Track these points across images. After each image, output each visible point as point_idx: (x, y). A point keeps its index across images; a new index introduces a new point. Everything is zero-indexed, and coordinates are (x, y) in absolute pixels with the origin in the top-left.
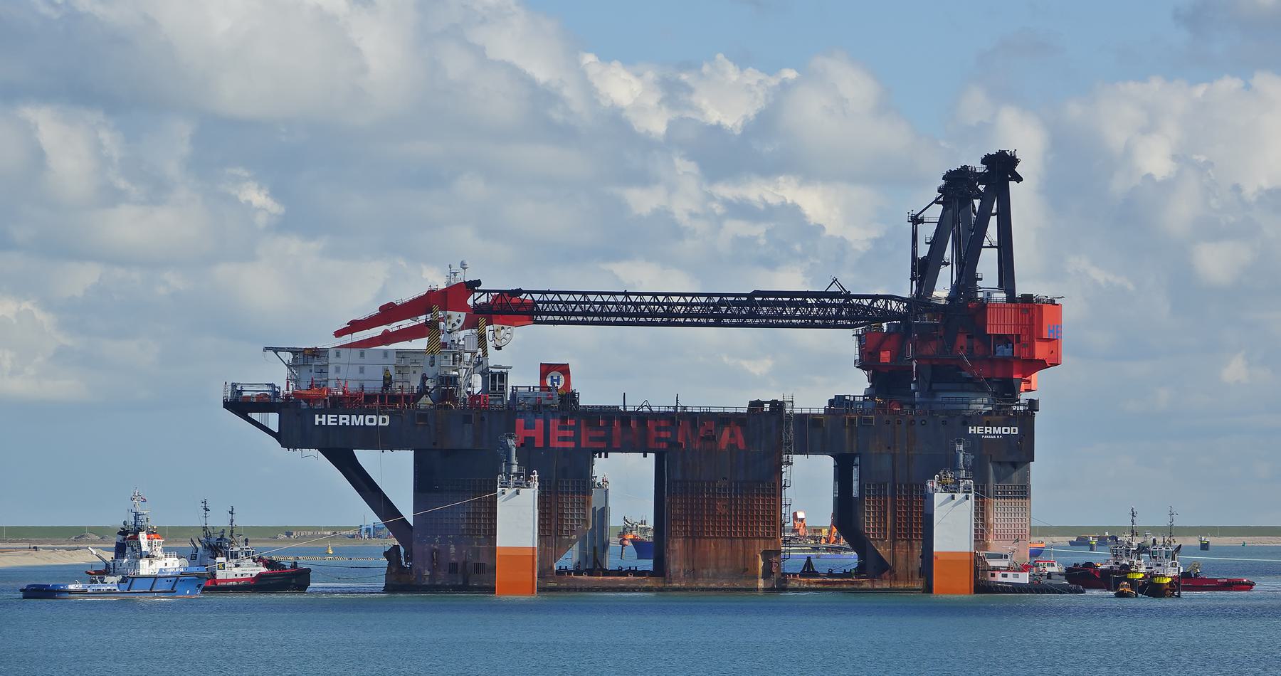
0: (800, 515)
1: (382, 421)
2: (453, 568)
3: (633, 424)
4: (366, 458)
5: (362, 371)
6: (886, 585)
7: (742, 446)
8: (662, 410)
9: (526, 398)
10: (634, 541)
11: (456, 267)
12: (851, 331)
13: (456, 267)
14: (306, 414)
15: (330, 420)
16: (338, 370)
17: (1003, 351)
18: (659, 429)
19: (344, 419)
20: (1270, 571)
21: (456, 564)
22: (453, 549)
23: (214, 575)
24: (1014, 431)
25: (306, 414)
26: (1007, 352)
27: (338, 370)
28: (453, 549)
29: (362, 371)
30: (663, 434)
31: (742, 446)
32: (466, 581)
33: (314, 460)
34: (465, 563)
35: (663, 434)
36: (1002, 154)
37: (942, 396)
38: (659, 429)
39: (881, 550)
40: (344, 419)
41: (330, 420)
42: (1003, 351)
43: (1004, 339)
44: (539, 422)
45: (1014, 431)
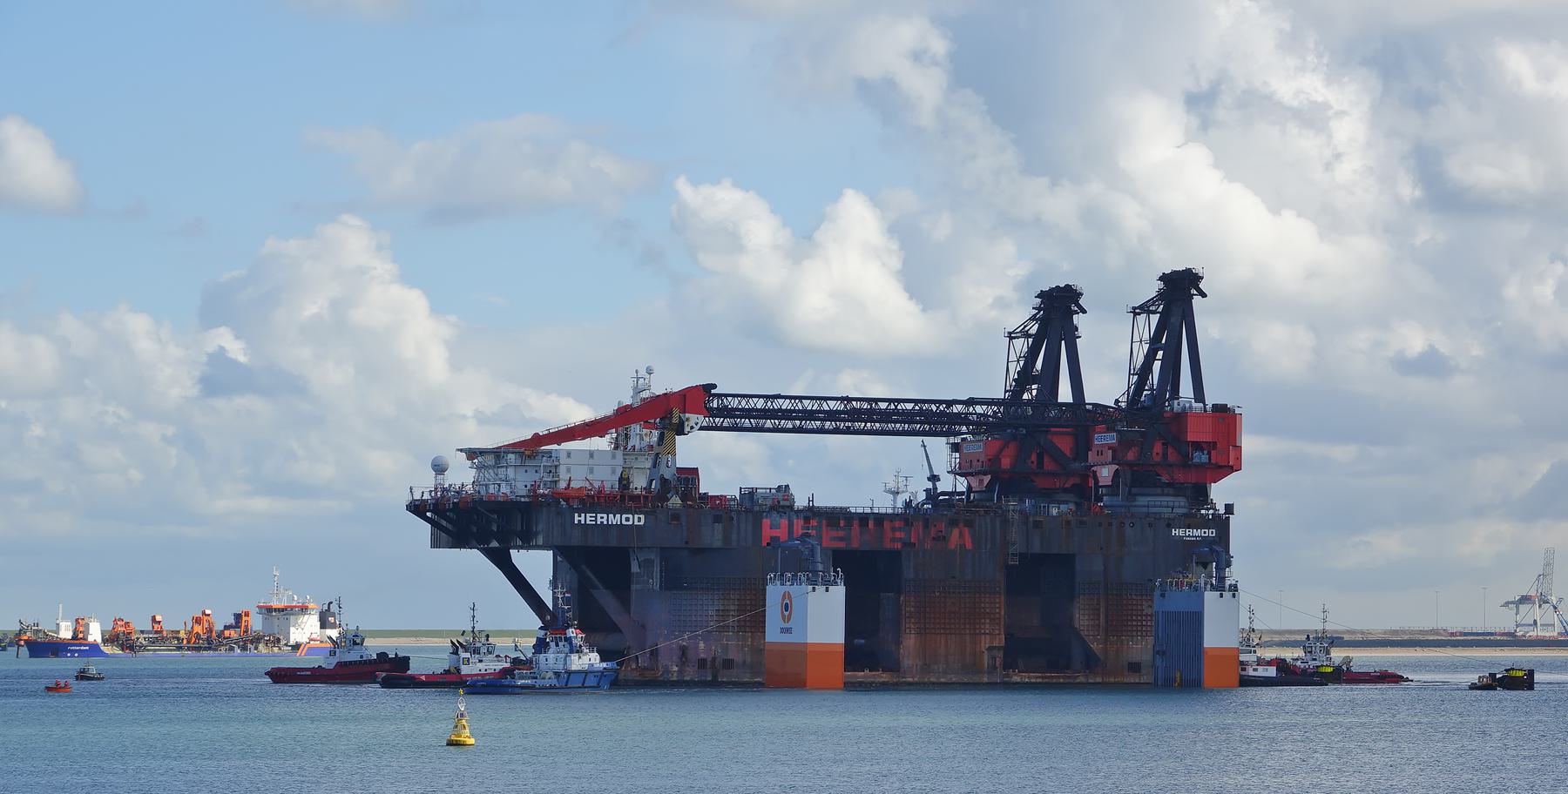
0: (158, 618)
1: (450, 527)
2: (702, 663)
3: (871, 523)
4: (520, 558)
5: (591, 471)
6: (1099, 680)
7: (969, 546)
8: (860, 511)
9: (765, 498)
10: (28, 642)
11: (643, 373)
12: (944, 439)
13: (643, 373)
14: (458, 520)
15: (589, 519)
16: (569, 470)
17: (1200, 457)
18: (893, 529)
19: (602, 518)
20: (1553, 666)
21: (704, 660)
22: (702, 645)
23: (458, 670)
24: (1211, 533)
25: (458, 520)
26: (1205, 458)
27: (569, 470)
28: (702, 645)
29: (591, 471)
30: (898, 535)
31: (969, 546)
32: (715, 677)
33: (473, 558)
34: (714, 659)
35: (898, 535)
36: (1188, 271)
37: (1142, 501)
38: (893, 529)
39: (1094, 646)
40: (602, 518)
41: (589, 519)
42: (1200, 457)
43: (1198, 446)
44: (785, 521)
45: (1211, 533)
